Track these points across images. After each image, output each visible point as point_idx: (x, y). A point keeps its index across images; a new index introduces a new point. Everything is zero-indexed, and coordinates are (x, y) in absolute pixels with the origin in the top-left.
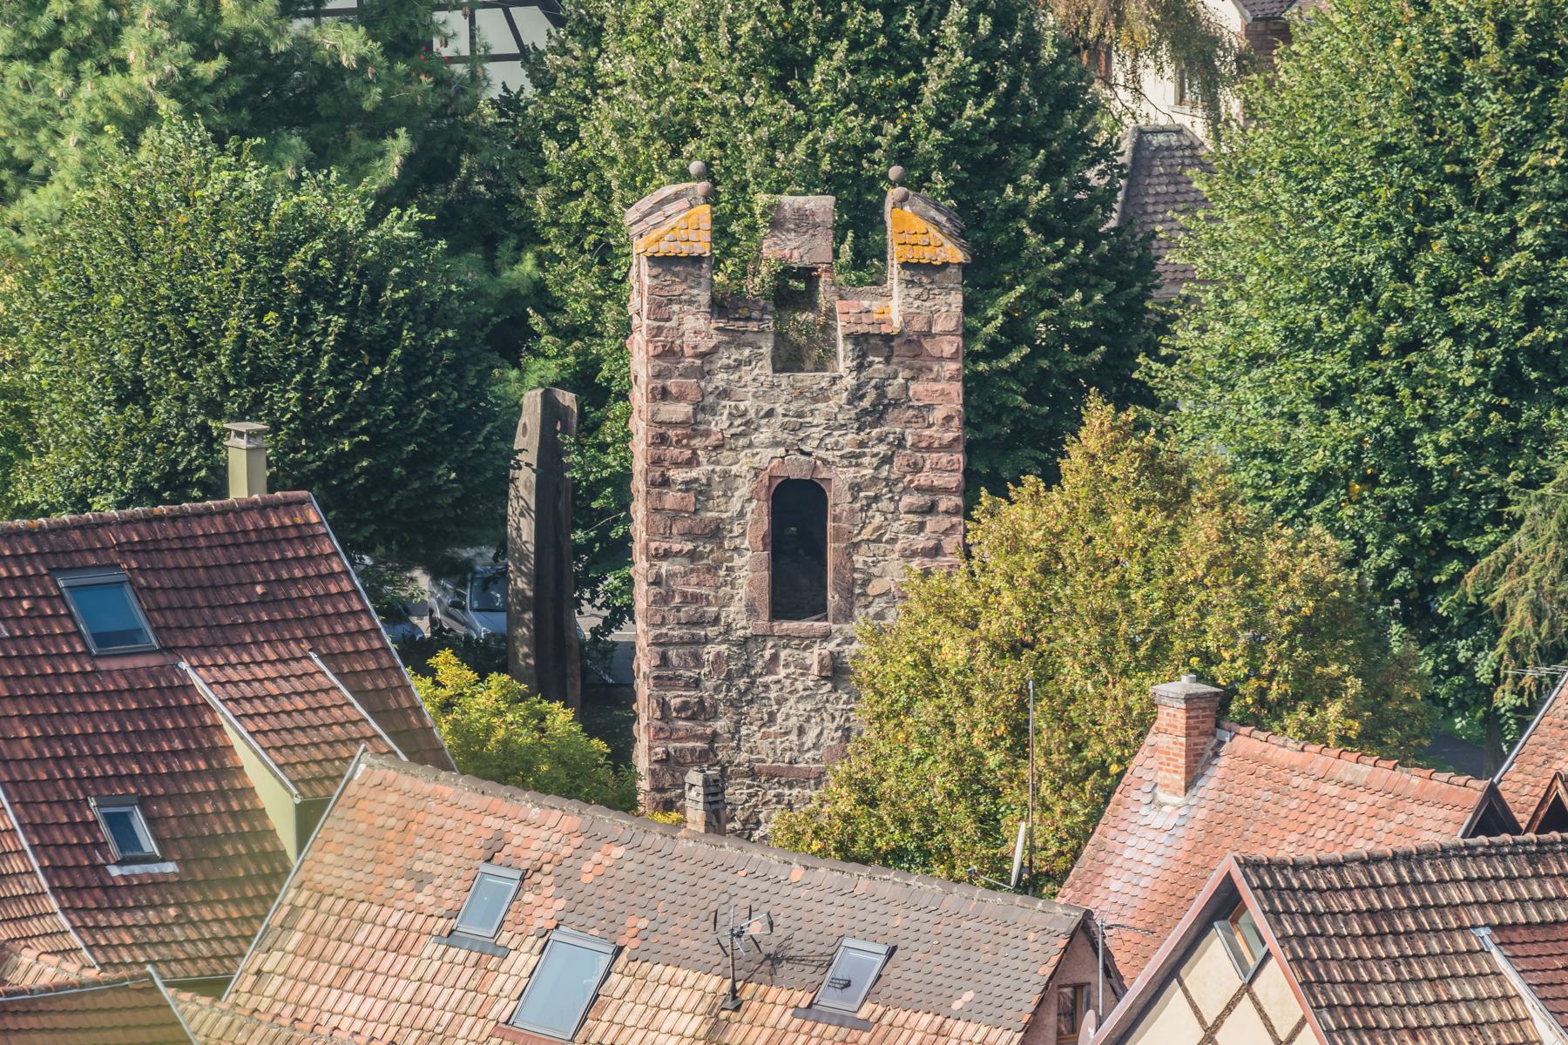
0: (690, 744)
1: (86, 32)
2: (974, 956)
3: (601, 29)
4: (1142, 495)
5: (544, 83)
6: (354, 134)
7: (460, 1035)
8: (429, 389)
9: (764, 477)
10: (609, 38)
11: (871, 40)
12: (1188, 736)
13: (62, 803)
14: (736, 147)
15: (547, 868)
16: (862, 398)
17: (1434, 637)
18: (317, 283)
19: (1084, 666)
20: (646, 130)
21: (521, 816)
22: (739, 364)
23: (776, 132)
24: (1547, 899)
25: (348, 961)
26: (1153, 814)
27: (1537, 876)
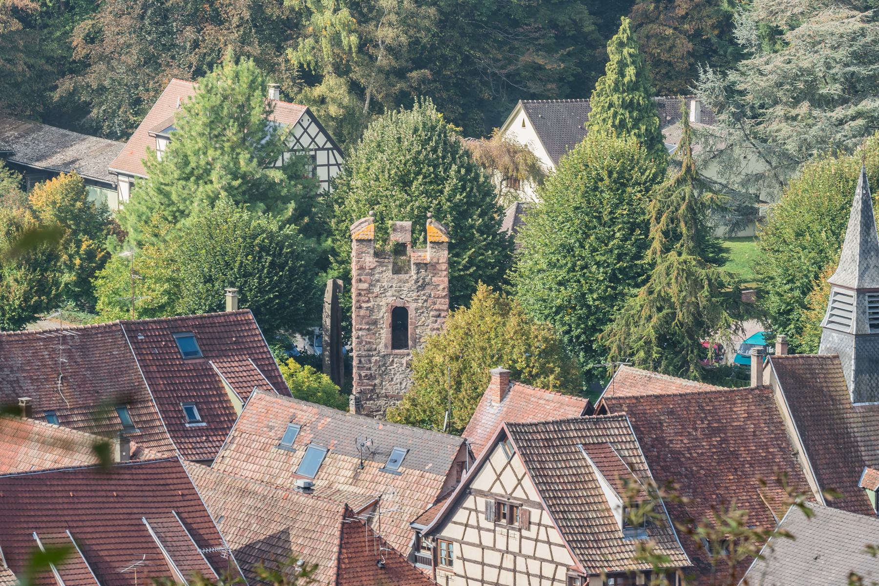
1: (201, 172)
6: (279, 202)
8: (297, 279)
10: (354, 174)
11: (430, 175)
13: (172, 404)
17: (594, 356)
20: (364, 202)
22: (382, 272)
24: (599, 436)
27: (596, 428)
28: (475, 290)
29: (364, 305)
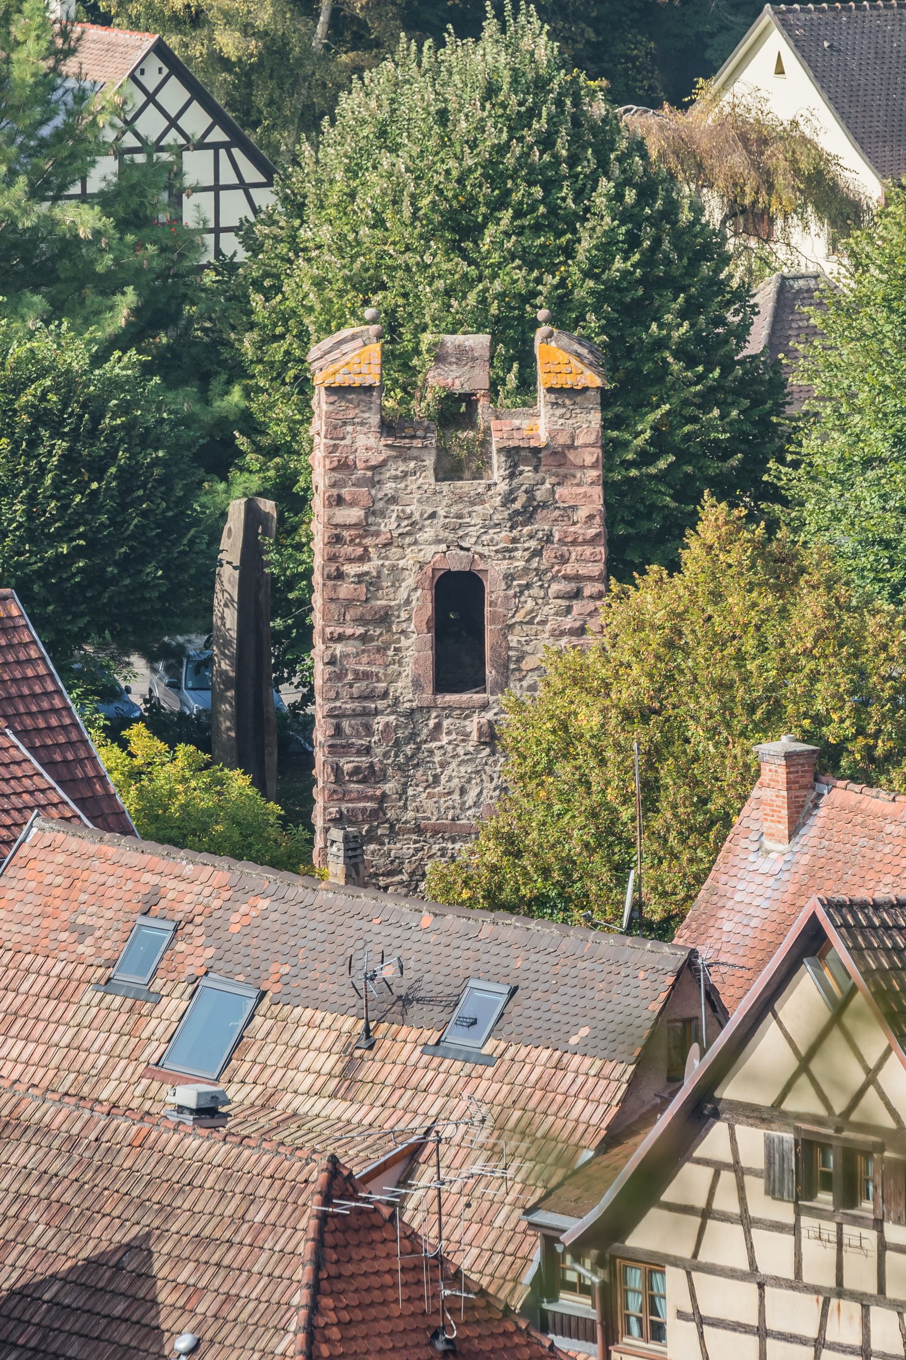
0: (361, 805)
2: (589, 994)
3: (303, 205)
4: (755, 579)
5: (254, 246)
7: (113, 1077)
8: (141, 500)
9: (428, 570)
10: (310, 211)
11: (533, 209)
12: (789, 789)
14: (417, 296)
15: (198, 920)
16: (514, 501)
18: (45, 414)
19: (708, 730)
20: (340, 285)
21: (177, 872)
22: (405, 474)
23: (452, 285)
25: (13, 1008)
26: (761, 860)
28: (693, 520)
29: (351, 569)
